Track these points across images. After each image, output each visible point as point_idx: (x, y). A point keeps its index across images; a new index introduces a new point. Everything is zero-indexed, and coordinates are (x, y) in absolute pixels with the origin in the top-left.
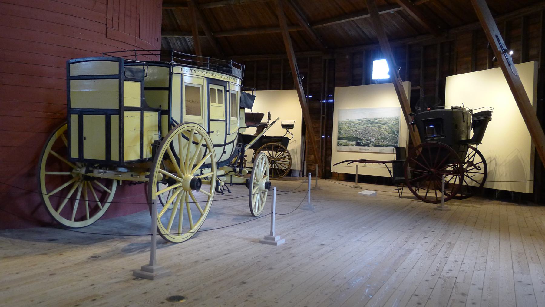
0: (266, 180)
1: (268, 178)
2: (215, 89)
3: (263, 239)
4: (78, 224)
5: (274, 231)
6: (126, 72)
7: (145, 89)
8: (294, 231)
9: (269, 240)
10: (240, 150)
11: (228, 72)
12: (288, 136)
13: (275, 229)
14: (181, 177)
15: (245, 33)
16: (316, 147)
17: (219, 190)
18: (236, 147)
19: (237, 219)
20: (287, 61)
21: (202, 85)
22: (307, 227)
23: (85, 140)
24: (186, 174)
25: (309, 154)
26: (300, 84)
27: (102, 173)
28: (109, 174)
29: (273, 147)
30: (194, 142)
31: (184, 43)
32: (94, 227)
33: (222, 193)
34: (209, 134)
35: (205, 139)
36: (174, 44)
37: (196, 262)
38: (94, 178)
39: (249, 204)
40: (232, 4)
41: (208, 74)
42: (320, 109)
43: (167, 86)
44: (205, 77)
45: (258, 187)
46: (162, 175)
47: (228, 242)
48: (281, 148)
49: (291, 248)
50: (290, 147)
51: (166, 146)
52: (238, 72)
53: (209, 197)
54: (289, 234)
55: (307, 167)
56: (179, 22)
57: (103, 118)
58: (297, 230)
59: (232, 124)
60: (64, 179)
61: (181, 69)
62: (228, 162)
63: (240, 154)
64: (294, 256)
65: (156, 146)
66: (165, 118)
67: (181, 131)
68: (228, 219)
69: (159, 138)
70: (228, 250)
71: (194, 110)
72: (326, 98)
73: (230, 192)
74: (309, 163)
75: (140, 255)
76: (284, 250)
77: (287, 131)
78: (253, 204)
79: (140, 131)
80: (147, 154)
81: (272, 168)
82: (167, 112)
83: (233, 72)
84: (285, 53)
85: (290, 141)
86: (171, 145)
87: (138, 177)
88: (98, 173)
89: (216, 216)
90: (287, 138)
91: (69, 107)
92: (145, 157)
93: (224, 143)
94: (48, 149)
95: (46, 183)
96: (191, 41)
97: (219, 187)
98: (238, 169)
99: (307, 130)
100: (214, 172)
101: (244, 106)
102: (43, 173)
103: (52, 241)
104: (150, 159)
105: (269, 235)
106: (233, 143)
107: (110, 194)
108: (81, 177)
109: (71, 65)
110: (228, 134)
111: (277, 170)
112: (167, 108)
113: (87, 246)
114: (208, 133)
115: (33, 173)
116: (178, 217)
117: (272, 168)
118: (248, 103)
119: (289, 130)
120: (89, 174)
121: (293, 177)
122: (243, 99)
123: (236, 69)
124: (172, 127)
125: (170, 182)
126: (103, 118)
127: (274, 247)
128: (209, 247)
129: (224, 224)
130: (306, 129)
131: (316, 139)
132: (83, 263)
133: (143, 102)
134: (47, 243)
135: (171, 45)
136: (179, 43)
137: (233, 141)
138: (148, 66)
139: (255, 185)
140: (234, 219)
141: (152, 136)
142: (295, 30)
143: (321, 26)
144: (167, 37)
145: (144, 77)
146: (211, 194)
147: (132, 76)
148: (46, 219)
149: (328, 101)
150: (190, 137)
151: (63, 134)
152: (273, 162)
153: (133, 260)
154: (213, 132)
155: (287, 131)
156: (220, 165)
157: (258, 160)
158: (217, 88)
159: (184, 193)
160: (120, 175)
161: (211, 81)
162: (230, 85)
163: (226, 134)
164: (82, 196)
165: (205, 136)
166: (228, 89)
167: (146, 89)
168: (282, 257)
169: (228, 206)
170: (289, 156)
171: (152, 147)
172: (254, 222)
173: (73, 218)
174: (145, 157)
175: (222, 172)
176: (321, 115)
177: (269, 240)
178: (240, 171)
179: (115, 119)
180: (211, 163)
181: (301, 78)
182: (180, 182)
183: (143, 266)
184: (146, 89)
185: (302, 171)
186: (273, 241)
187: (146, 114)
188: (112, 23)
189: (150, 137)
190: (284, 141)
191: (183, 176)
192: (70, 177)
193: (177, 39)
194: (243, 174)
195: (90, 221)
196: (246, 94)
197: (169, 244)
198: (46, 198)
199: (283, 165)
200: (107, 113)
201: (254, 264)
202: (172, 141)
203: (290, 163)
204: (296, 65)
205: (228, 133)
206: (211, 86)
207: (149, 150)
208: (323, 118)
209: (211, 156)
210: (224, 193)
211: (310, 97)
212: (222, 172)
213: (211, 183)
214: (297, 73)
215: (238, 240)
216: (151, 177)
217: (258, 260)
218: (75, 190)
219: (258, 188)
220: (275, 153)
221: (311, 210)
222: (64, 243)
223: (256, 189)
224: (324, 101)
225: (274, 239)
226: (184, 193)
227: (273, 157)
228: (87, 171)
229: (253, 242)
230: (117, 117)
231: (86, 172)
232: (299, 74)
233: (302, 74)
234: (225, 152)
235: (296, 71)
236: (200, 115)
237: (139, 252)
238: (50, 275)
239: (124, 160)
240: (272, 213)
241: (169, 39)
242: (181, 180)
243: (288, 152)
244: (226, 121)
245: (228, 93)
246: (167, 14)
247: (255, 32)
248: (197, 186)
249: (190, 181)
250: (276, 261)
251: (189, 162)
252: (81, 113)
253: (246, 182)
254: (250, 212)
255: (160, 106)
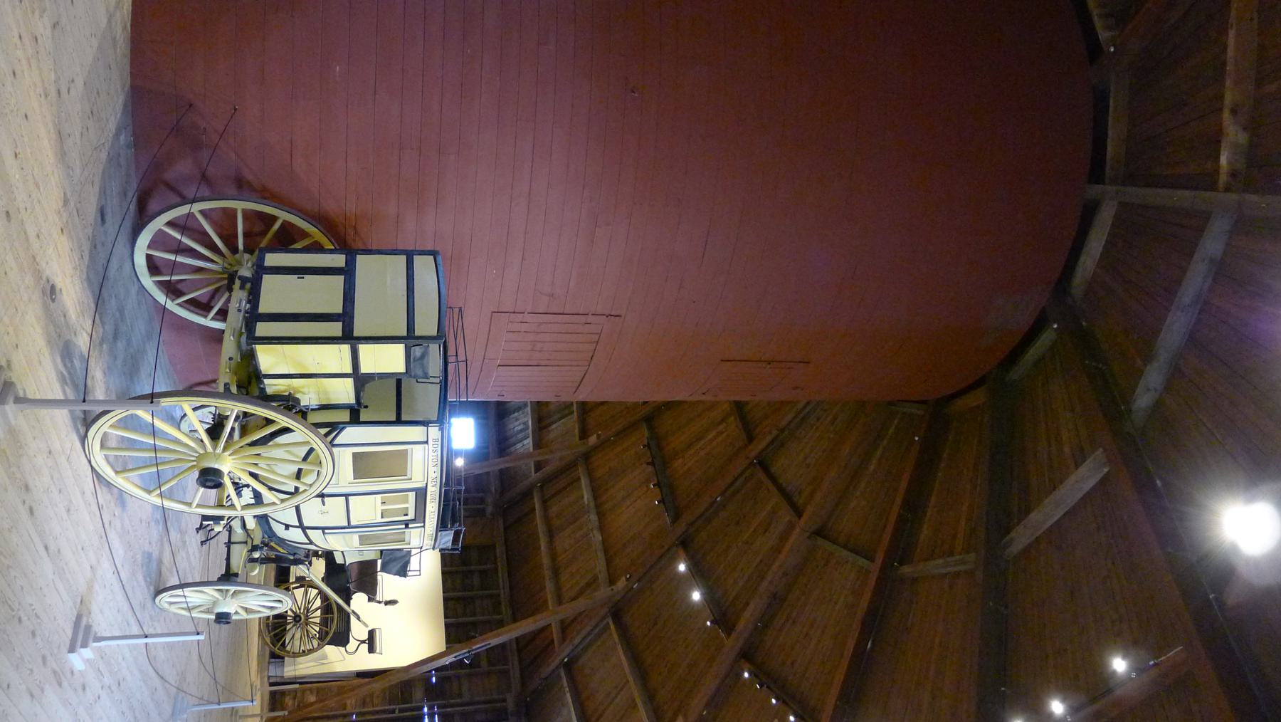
0: (237, 613)
1: (242, 615)
2: (407, 502)
3: (88, 622)
4: (140, 261)
5: (103, 643)
6: (421, 348)
7: (398, 381)
8: (109, 687)
9: (82, 634)
10: (297, 557)
11: (442, 525)
12: (352, 645)
13: (118, 645)
14: (225, 449)
15: (543, 543)
16: (332, 703)
17: (205, 523)
18: (304, 549)
19: (150, 561)
20: (501, 624)
21: (411, 479)
22: (123, 713)
23: (298, 278)
24: (233, 463)
25: (318, 690)
26: (455, 657)
27: (238, 305)
28: (236, 319)
29: (329, 616)
30: (300, 470)
31: (521, 436)
32: (134, 290)
33: (201, 527)
34: (318, 496)
35: (305, 491)
36: (517, 420)
37: (27, 488)
38: (230, 290)
39: (192, 581)
40: (589, 516)
41: (434, 489)
42: (411, 703)
43: (404, 418)
44: (427, 484)
45: (220, 598)
46: (228, 413)
47: (83, 549)
48: (327, 633)
49: (60, 684)
50: (330, 650)
51: (283, 420)
52: (446, 542)
53: (190, 504)
54: (102, 675)
55: (290, 691)
56: (554, 426)
57: (339, 309)
58: (112, 692)
59: (344, 539)
60: (230, 240)
61: (436, 440)
62: (272, 534)
63: (292, 558)
64: (32, 695)
65: (289, 404)
66: (345, 416)
67: (315, 446)
68: (150, 543)
69: (304, 406)
70: (59, 551)
71: (365, 465)
72: (430, 712)
73: (202, 545)
74: (298, 695)
75: (53, 376)
76: (55, 672)
77: (363, 642)
78: (187, 591)
79: (315, 373)
80: (272, 386)
81: (288, 618)
82: (355, 420)
83: (444, 533)
84: (515, 620)
85: (342, 649)
86: (286, 430)
87: (228, 370)
88: (239, 297)
89: (159, 517)
90: (348, 642)
91: (359, 252)
92: (266, 381)
93: (305, 525)
94: (283, 216)
95: (224, 210)
96: (525, 447)
97: (212, 522)
98: (256, 555)
99: (367, 680)
100: (241, 510)
101: (384, 558)
102: (239, 206)
103: (99, 215)
104: (263, 390)
105: (96, 634)
106: (308, 542)
107: (206, 317)
108: (235, 269)
109: (432, 257)
110: (324, 533)
111: (282, 628)
112: (362, 419)
113: (84, 276)
114: (322, 496)
115: (242, 187)
116: (144, 447)
117: (288, 618)
118: (391, 565)
119: (365, 646)
120: (238, 283)
121: (269, 663)
122: (398, 554)
123: (451, 537)
124: (323, 431)
125: (215, 431)
126: (339, 309)
127: (65, 649)
128: (68, 511)
129: (135, 536)
130: (370, 679)
131: (349, 702)
132: (38, 274)
133: (370, 377)
134: (95, 204)
135: (516, 414)
136: (519, 428)
137: (311, 543)
138: (439, 385)
139: (224, 593)
140: (150, 555)
141: (309, 395)
142: (555, 636)
143: (565, 684)
144: (527, 406)
145: (414, 378)
146: (196, 507)
147: (414, 358)
148: (153, 206)
149: (426, 717)
150: (310, 463)
151: (313, 240)
152: (298, 619)
153: (40, 363)
154: (324, 503)
155: (363, 642)
156: (263, 520)
157: (277, 594)
158: (411, 505)
159: (193, 456)
160: (232, 338)
161: (421, 494)
162: (419, 529)
163: (323, 529)
164: (199, 270)
165: (313, 489)
166: (410, 526)
167: (399, 383)
168: (31, 670)
169: (187, 538)
170: (310, 651)
171: (287, 394)
172: (141, 592)
173: (151, 252)
174: (266, 381)
175: (251, 524)
176: (398, 706)
177: (82, 634)
178: (253, 560)
179: (336, 329)
180: (265, 503)
181: (466, 658)
182: (215, 448)
183: (15, 385)
184: (399, 383)
185: (283, 681)
186: (79, 643)
187: (349, 382)
188: (519, 321)
189: (305, 390)
190: (341, 638)
191: (227, 454)
192: (234, 250)
193: (525, 423)
194: (249, 565)
195: (148, 281)
196: (407, 559)
197: (82, 430)
198: (196, 208)
199: (294, 638)
200: (346, 317)
201: (13, 610)
202: (294, 431)
203: (295, 655)
204: (489, 644)
205: (326, 531)
206: (412, 495)
207: (282, 388)
208: (393, 712)
209: (274, 504)
210: (201, 532)
211: (434, 679)
212: (251, 524)
213: (220, 506)
214: (474, 648)
215: (89, 568)
216: (227, 394)
217: (24, 618)
218: (221, 251)
219: (218, 599)
220: (318, 620)
221: (173, 714)
222: (94, 236)
223: (217, 595)
224: (426, 710)
225: (84, 645)
226: (193, 456)
227: (310, 618)
228: (244, 280)
229: (81, 602)
230: (340, 334)
231: (240, 278)
232: (473, 653)
233: (476, 659)
234: (288, 529)
235: (478, 646)
236: (354, 479)
237: (62, 373)
238: (8, 212)
239: (257, 346)
240: (146, 637)
241: (526, 410)
242: (219, 450)
243: (320, 647)
244: (349, 526)
245: (404, 526)
246: (565, 408)
247: (546, 561)
248: (207, 480)
249: (216, 466)
250: (22, 658)
251: (262, 464)
252: (348, 272)
253: (231, 572)
254: (168, 586)
255: (366, 407)
